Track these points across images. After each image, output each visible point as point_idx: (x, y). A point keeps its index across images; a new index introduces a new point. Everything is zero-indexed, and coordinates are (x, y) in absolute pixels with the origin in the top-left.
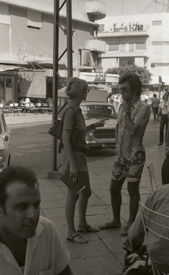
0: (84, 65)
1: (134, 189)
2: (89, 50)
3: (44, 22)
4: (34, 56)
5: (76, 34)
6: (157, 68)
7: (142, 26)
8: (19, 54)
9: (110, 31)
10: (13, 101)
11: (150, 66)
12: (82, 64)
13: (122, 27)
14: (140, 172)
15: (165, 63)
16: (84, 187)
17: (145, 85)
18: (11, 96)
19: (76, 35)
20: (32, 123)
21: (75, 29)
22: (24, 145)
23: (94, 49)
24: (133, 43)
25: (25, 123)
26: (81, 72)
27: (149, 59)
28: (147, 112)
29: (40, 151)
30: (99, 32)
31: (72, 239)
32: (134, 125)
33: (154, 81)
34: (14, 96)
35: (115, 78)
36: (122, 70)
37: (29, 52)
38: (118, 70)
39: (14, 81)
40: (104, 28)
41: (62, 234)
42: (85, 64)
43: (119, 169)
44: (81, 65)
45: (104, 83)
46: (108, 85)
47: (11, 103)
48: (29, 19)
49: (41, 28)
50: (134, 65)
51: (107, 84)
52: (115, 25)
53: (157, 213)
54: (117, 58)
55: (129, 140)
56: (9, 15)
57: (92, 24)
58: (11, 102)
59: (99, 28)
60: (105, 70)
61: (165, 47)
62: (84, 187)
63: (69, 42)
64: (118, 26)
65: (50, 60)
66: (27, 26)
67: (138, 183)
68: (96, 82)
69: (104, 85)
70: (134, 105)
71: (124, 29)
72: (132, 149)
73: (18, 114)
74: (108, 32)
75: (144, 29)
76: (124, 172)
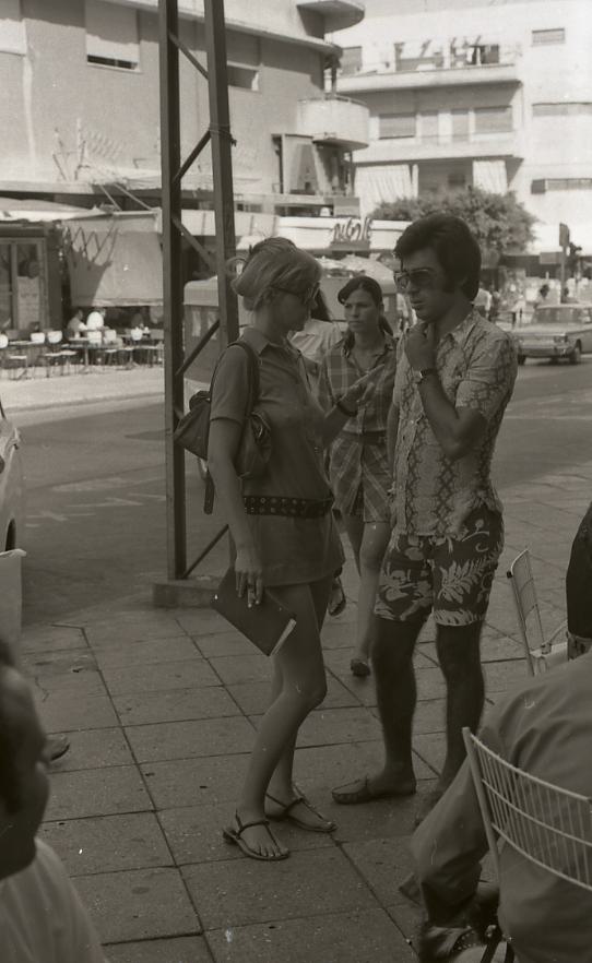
0: (294, 192)
1: (461, 653)
2: (311, 137)
3: (143, 43)
4: (113, 162)
5: (259, 82)
6: (551, 196)
7: (496, 48)
8: (61, 159)
9: (381, 68)
10: (43, 323)
11: (529, 189)
12: (285, 189)
13: (423, 53)
14: (484, 589)
15: (580, 179)
16: (292, 623)
17: (510, 257)
18: (37, 307)
19: (259, 87)
20: (111, 398)
21: (258, 64)
22: (78, 481)
23: (326, 134)
24: (465, 111)
25: (87, 402)
26: (283, 215)
27: (524, 163)
28: (503, 360)
29: (131, 503)
30: (341, 74)
31: (240, 831)
32: (457, 417)
33: (544, 242)
34: (48, 306)
36: (430, 206)
37: (94, 150)
38: (416, 208)
39: (45, 254)
40: (361, 60)
41: (196, 827)
42: (295, 188)
43: (404, 579)
44: (282, 192)
45: (365, 254)
46: (379, 260)
47: (38, 331)
48: (93, 33)
49: (136, 64)
50: (470, 188)
51: (378, 255)
52: (398, 48)
53: (536, 779)
54: (410, 163)
55: (438, 468)
56: (21, 20)
57: (316, 45)
58: (36, 328)
59: (342, 61)
60: (367, 207)
61: (580, 121)
62: (292, 623)
63: (215, 104)
64: (410, 52)
65: (149, 174)
66: (86, 58)
67: (471, 633)
68: (336, 249)
69: (365, 260)
70: (454, 334)
71: (431, 60)
72: (449, 502)
73: (62, 369)
74: (374, 72)
75: (503, 59)
76: (423, 587)
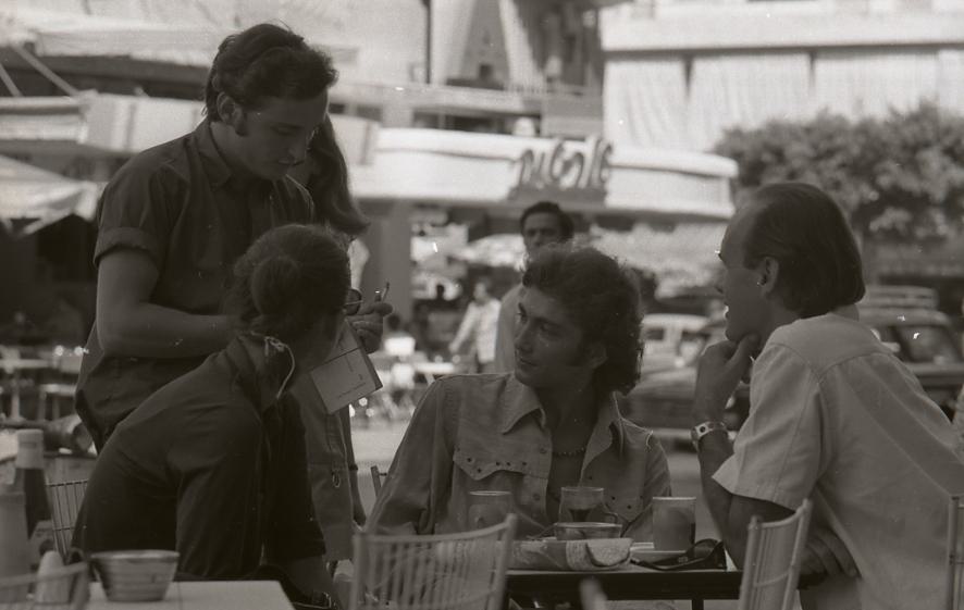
0: (454, 83)
12: (438, 73)
35: (692, 183)
42: (455, 73)
44: (428, 81)
